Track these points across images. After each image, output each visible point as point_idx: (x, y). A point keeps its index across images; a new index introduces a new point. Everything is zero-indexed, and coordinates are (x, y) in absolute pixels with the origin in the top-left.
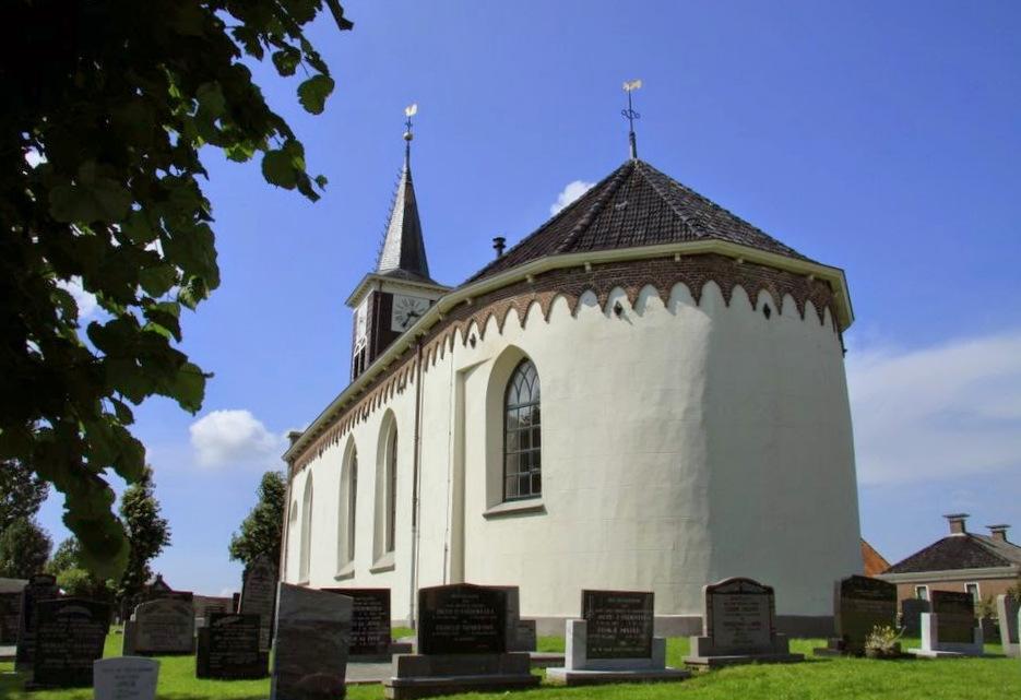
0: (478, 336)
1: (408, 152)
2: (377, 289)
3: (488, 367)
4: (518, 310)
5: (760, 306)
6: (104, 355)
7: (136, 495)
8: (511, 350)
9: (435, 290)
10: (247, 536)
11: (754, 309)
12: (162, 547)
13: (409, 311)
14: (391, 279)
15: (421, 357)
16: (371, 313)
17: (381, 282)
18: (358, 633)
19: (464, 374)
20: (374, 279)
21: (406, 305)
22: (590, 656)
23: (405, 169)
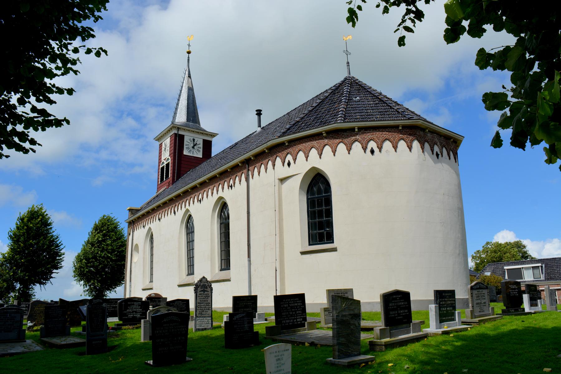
0: (292, 162)
2: (176, 132)
4: (317, 149)
5: (435, 153)
8: (313, 169)
11: (433, 154)
20: (174, 126)
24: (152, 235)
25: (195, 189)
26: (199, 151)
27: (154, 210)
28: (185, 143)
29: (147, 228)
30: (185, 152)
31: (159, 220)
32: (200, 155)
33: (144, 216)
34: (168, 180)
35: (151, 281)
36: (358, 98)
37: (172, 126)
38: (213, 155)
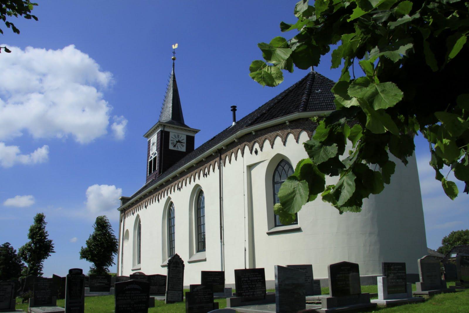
0: (259, 149)
1: (174, 65)
3: (266, 164)
4: (281, 137)
6: (449, 141)
7: (36, 228)
8: (278, 155)
9: (188, 130)
10: (89, 247)
12: (50, 254)
13: (177, 140)
14: (169, 125)
15: (221, 159)
16: (159, 141)
17: (164, 126)
18: (253, 291)
19: (250, 167)
20: (161, 124)
21: (176, 137)
22: (389, 293)
23: (172, 73)
24: (140, 222)
25: (175, 178)
26: (183, 146)
27: (141, 199)
28: (171, 139)
29: (136, 214)
30: (171, 147)
31: (146, 207)
32: (183, 149)
33: (133, 204)
34: (155, 173)
35: (139, 262)
36: (320, 90)
37: (158, 123)
38: (195, 149)
